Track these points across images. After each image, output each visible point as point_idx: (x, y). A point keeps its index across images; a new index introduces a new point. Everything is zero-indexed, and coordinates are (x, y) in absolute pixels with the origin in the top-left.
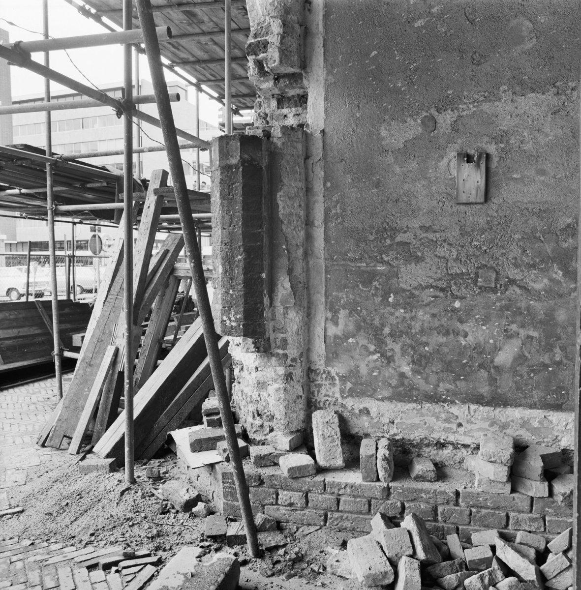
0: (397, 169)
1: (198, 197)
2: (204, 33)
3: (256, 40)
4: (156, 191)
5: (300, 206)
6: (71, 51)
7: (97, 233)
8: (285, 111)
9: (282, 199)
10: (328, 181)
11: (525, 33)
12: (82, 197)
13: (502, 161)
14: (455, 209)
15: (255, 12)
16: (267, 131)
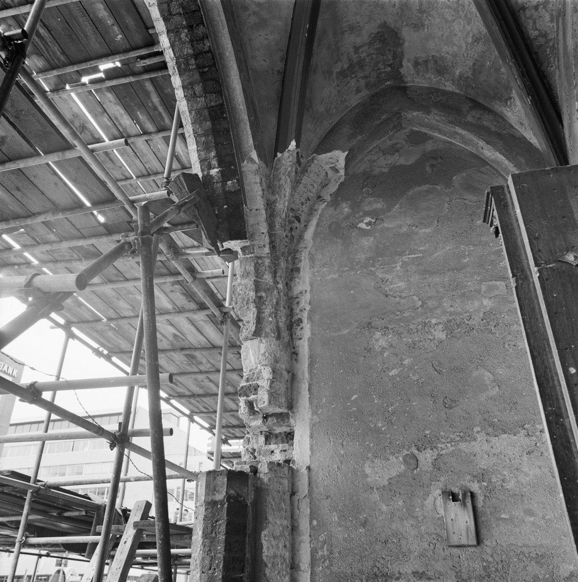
0: (384, 508)
1: (179, 532)
2: (201, 372)
3: (248, 384)
4: (136, 525)
5: (285, 546)
6: (78, 391)
7: (62, 568)
8: (272, 447)
9: (266, 538)
10: (314, 519)
11: (488, 382)
12: (56, 526)
13: (487, 500)
14: (447, 552)
15: (248, 360)
16: (255, 467)
